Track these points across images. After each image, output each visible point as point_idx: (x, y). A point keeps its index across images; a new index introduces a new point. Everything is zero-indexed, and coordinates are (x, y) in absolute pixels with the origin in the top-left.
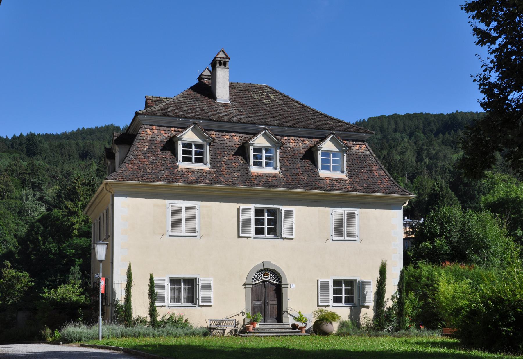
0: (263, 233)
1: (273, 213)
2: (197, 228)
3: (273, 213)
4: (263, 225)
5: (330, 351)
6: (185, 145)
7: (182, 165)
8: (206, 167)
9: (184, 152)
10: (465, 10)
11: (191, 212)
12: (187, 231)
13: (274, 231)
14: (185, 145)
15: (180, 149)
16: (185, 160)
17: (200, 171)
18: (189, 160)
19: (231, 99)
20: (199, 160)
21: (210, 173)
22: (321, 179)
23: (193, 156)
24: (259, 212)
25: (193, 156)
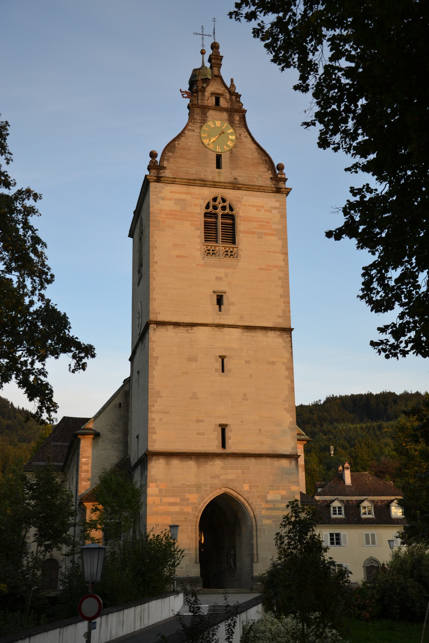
0: (334, 544)
1: (338, 535)
2: (376, 543)
3: (338, 535)
4: (334, 540)
5: (152, 601)
6: (334, 508)
7: (333, 516)
8: (342, 516)
9: (333, 511)
10: (315, 95)
11: (373, 535)
12: (372, 544)
13: (338, 543)
14: (334, 508)
15: (332, 509)
16: (335, 514)
17: (341, 519)
18: (336, 514)
19: (352, 483)
20: (340, 514)
21: (343, 519)
22: (393, 519)
23: (337, 512)
24: (332, 535)
25: (337, 512)
